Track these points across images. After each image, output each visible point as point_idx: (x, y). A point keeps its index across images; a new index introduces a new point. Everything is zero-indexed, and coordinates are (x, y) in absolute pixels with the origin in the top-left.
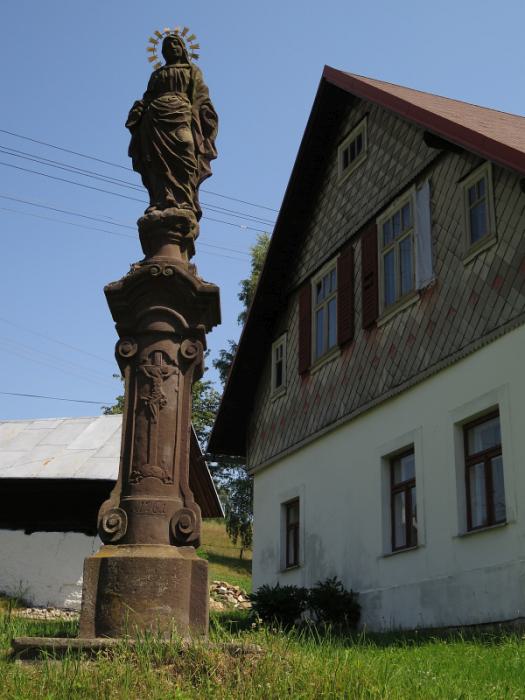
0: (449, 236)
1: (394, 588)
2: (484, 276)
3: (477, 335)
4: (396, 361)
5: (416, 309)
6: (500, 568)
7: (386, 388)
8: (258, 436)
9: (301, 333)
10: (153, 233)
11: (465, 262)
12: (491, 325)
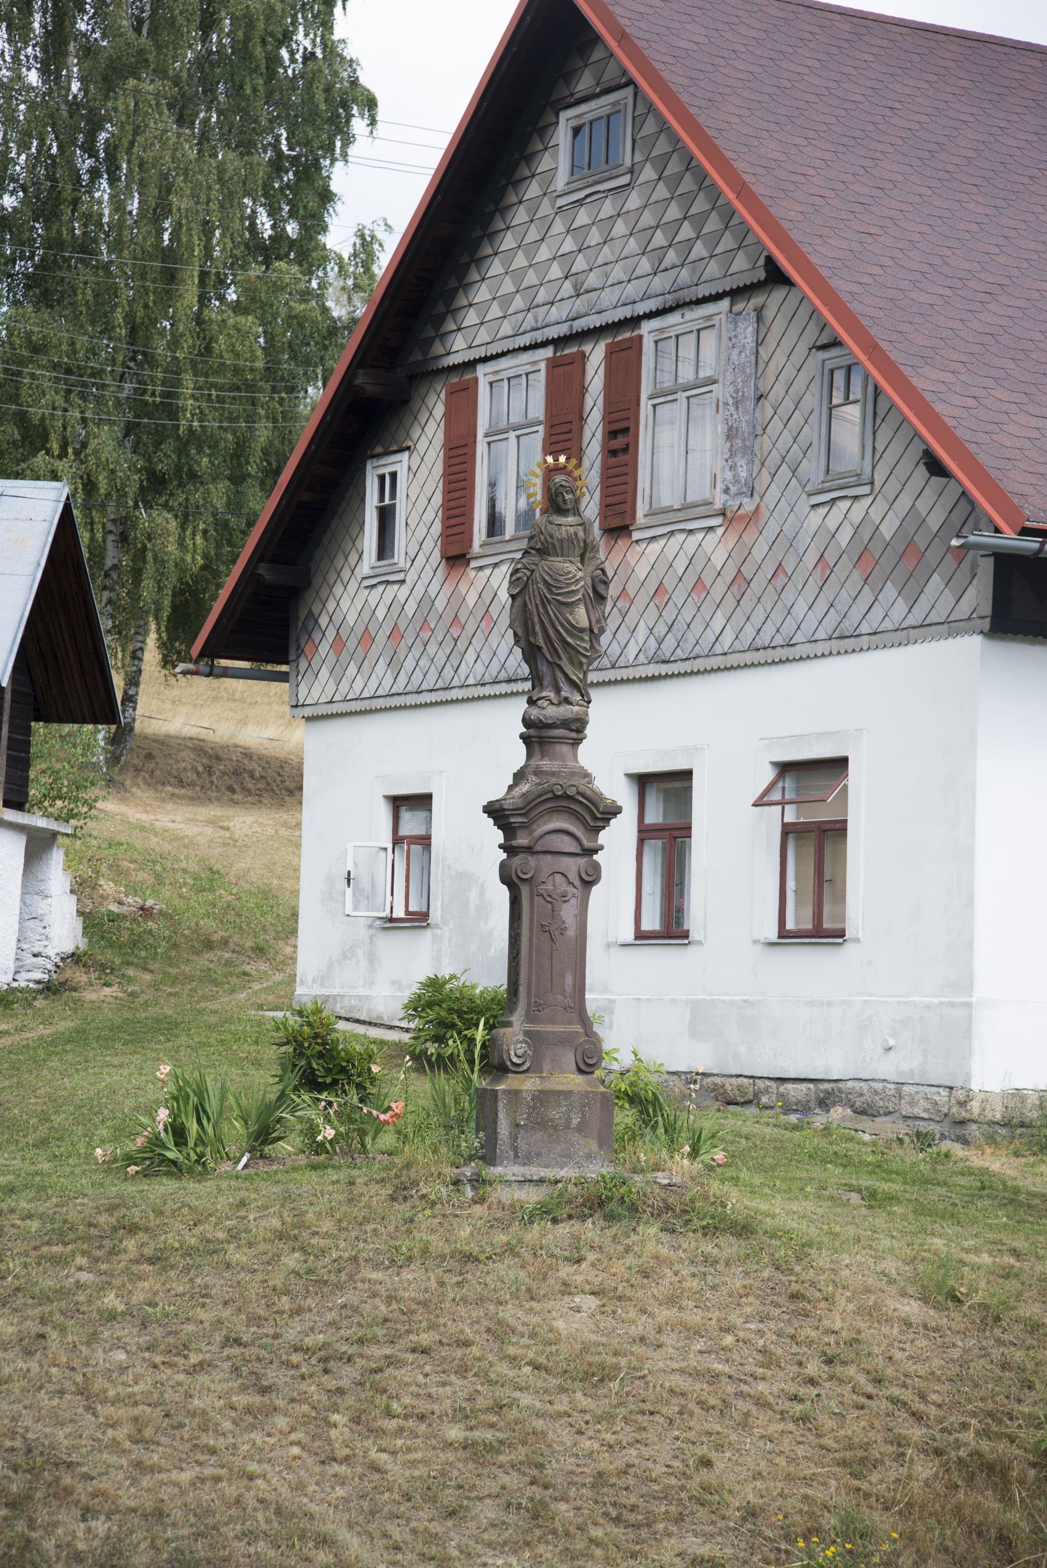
0: (786, 438)
1: (638, 999)
2: (844, 537)
3: (821, 634)
4: (669, 615)
5: (712, 538)
6: (829, 1004)
7: (642, 658)
8: (324, 649)
9: (448, 464)
10: (537, 736)
11: (815, 500)
12: (848, 626)
